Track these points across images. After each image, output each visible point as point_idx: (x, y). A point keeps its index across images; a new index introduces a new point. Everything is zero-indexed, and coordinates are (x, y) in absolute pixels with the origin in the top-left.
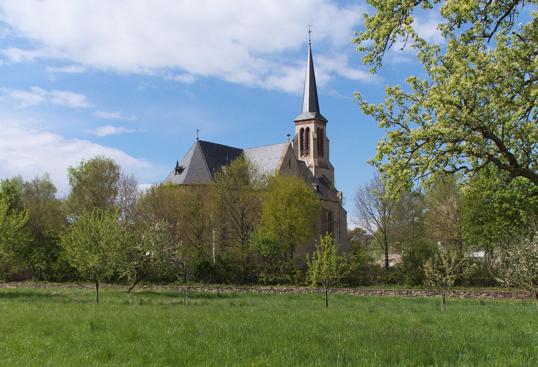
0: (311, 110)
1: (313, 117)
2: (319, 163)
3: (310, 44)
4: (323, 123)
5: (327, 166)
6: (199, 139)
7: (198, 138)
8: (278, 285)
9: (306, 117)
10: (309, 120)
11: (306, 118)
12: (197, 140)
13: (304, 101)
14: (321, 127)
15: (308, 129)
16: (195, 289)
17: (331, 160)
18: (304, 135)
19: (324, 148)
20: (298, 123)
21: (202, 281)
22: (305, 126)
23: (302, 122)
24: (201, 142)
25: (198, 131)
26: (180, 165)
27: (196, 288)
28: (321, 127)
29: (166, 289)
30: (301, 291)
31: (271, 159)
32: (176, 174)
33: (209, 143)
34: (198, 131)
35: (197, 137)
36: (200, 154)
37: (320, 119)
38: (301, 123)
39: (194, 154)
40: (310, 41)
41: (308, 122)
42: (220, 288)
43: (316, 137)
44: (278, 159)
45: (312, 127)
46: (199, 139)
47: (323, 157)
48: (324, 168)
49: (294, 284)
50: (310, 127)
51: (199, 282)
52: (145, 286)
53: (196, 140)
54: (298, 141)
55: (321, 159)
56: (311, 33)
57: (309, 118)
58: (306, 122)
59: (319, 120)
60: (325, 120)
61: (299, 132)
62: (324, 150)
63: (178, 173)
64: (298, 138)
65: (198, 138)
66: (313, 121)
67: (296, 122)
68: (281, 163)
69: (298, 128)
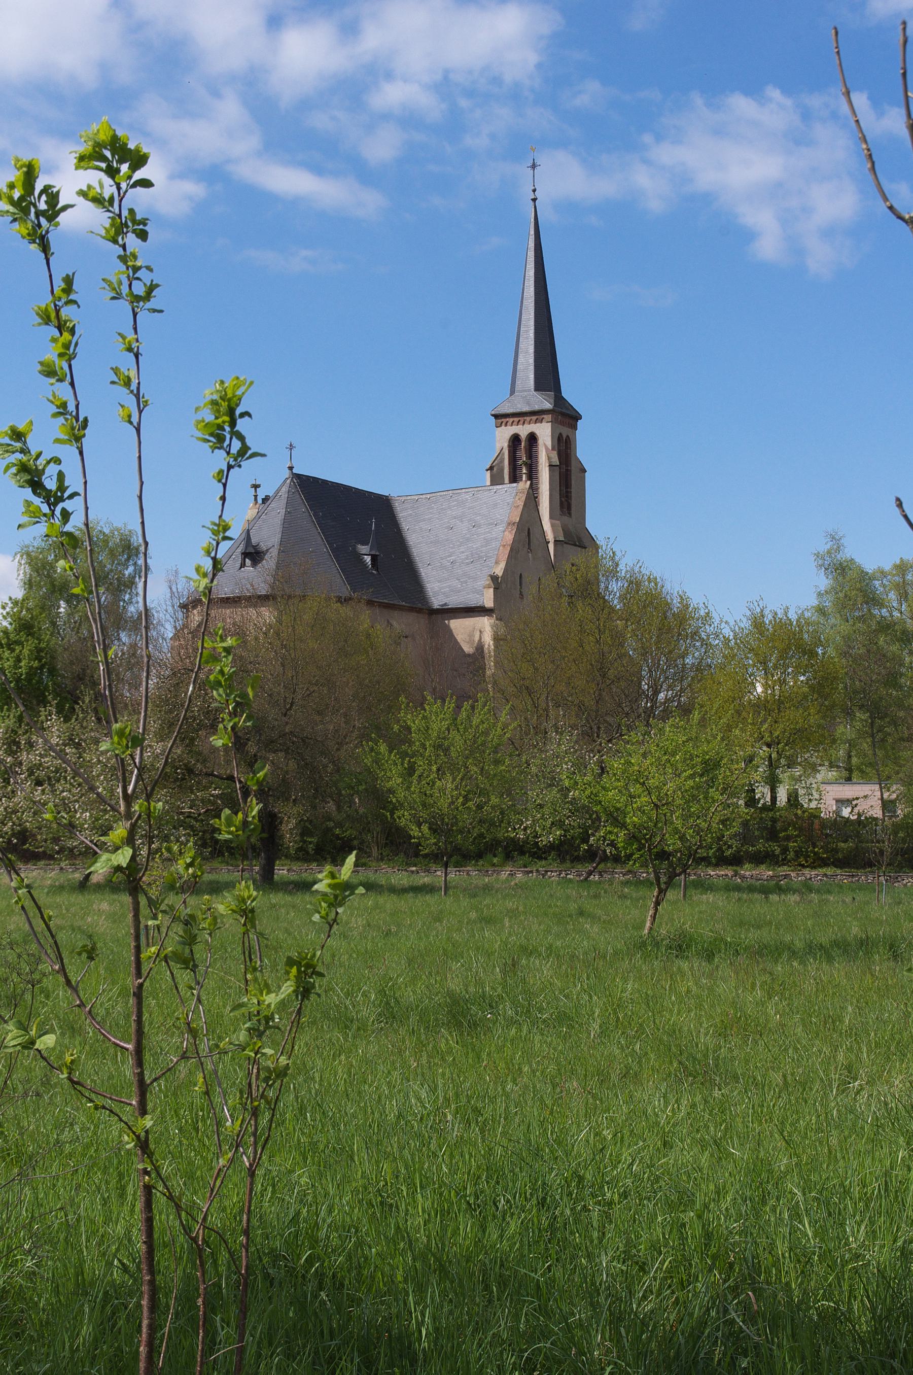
0: (539, 387)
1: (548, 406)
2: (566, 532)
3: (534, 200)
4: (571, 421)
5: (580, 539)
6: (295, 471)
7: (291, 468)
8: (747, 866)
9: (528, 404)
10: (537, 415)
11: (526, 409)
12: (288, 471)
13: (521, 359)
14: (565, 431)
15: (532, 438)
16: (544, 876)
17: (589, 525)
18: (523, 456)
19: (573, 490)
20: (504, 420)
21: (402, 855)
22: (523, 431)
23: (516, 419)
24: (298, 476)
25: (291, 447)
26: (254, 541)
27: (547, 872)
28: (565, 431)
29: (468, 874)
30: (811, 879)
31: (479, 526)
32: (243, 565)
33: (316, 479)
34: (291, 447)
35: (288, 465)
36: (303, 509)
37: (564, 411)
38: (511, 420)
39: (287, 513)
40: (534, 191)
41: (534, 418)
42: (606, 872)
43: (556, 461)
44: (501, 528)
45: (544, 432)
46: (295, 471)
47: (570, 514)
48: (575, 545)
49: (785, 862)
50: (538, 433)
51: (546, 859)
52: (414, 869)
53: (287, 473)
54: (502, 470)
55: (566, 519)
56: (537, 170)
57: (537, 408)
58: (528, 419)
59: (563, 414)
60: (574, 413)
61: (506, 445)
62: (573, 495)
63: (248, 562)
64: (502, 461)
65: (291, 468)
66: (548, 417)
67: (496, 416)
68: (509, 537)
69: (503, 435)
